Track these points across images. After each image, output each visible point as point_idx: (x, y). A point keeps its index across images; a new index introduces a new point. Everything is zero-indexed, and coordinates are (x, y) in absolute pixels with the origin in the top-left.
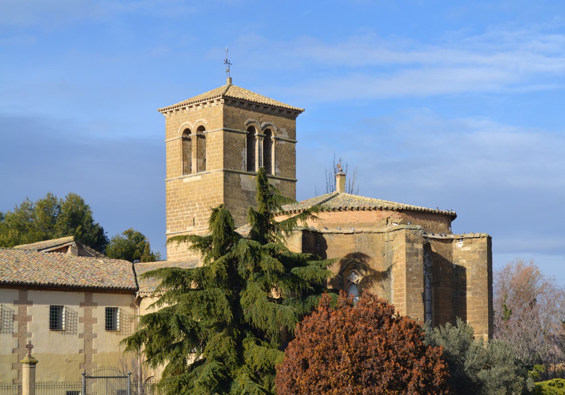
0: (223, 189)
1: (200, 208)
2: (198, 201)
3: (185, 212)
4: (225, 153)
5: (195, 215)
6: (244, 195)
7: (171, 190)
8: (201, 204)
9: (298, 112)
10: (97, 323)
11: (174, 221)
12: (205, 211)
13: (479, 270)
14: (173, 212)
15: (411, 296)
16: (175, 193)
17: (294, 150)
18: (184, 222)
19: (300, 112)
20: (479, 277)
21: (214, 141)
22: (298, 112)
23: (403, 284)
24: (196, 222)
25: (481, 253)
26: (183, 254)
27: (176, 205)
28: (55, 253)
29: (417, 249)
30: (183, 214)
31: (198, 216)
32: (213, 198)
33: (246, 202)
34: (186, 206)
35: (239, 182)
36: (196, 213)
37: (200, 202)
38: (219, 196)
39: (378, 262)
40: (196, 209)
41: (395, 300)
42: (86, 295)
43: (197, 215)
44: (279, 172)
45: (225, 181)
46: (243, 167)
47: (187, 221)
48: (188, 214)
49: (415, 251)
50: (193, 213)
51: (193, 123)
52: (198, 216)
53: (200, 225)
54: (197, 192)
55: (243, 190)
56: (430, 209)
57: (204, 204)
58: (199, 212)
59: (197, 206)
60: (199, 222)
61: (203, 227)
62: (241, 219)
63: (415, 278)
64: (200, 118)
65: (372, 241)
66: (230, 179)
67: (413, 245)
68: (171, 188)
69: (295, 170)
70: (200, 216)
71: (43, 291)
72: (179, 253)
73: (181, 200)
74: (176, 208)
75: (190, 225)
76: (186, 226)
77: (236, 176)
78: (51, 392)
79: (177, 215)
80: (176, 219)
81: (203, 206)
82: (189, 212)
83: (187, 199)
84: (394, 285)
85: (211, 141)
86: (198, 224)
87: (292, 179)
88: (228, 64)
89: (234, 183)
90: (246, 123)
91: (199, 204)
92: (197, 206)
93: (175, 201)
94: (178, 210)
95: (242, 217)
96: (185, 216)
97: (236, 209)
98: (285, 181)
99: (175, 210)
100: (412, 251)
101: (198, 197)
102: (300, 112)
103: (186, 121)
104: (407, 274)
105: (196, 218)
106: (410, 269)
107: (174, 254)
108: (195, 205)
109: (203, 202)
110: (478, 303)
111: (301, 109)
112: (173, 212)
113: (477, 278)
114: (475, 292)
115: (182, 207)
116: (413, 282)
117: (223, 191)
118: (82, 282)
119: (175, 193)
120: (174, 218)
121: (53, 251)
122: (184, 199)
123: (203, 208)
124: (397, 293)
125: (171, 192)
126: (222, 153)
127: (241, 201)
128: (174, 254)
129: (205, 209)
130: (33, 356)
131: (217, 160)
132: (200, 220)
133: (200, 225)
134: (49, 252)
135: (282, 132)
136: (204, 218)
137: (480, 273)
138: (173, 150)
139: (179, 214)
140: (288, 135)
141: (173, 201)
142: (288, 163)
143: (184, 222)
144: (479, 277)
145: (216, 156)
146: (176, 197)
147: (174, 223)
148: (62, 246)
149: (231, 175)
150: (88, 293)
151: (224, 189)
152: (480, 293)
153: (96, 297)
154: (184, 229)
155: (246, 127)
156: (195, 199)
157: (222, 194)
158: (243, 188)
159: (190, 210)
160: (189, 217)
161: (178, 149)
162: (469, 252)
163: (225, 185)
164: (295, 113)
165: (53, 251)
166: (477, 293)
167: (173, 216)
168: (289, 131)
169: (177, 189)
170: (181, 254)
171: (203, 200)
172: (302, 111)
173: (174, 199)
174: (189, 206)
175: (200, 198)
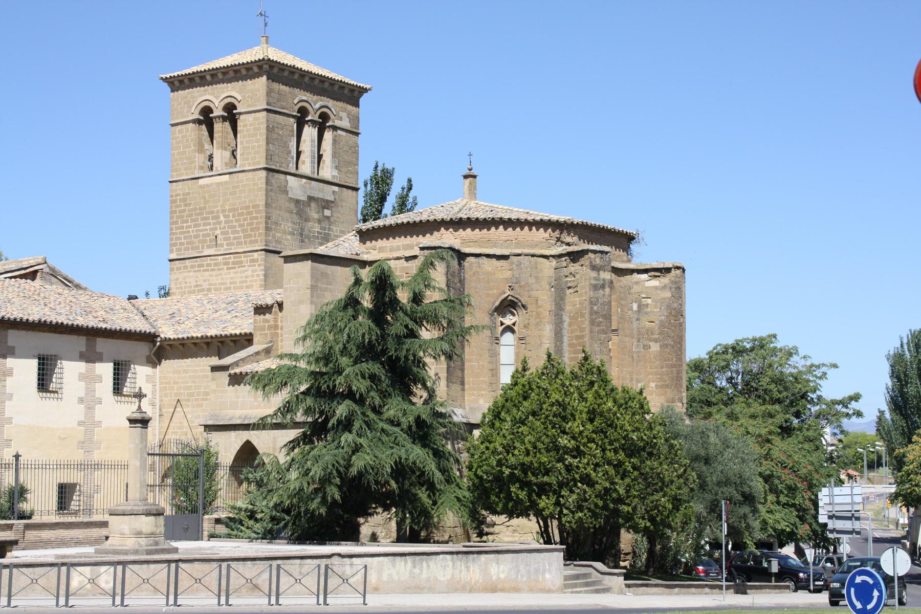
0: (264, 195)
1: (226, 222)
2: (223, 211)
3: (201, 228)
4: (268, 143)
5: (218, 232)
6: (292, 206)
7: (179, 195)
8: (228, 216)
9: (363, 91)
10: (101, 382)
11: (183, 241)
12: (235, 227)
13: (670, 313)
14: (182, 227)
15: (596, 345)
16: (184, 200)
17: (357, 145)
18: (199, 242)
19: (366, 90)
20: (670, 323)
21: (251, 125)
22: (363, 91)
23: (584, 328)
24: (219, 242)
25: (673, 289)
26: (197, 289)
27: (187, 217)
28: (18, 279)
29: (604, 280)
30: (197, 231)
31: (222, 233)
32: (248, 207)
33: (294, 216)
34: (193, 221)
35: (286, 186)
36: (220, 228)
37: (227, 213)
38: (258, 206)
39: (543, 297)
40: (220, 223)
41: (570, 351)
42: (87, 340)
43: (221, 232)
44: (337, 174)
45: (267, 183)
46: (291, 165)
47: (205, 241)
48: (206, 230)
49: (601, 282)
50: (216, 228)
51: (217, 98)
52: (222, 233)
53: (225, 247)
54: (221, 199)
55: (291, 198)
56: (609, 227)
57: (234, 216)
58: (224, 228)
59: (222, 218)
60: (225, 243)
61: (231, 249)
62: (287, 239)
63: (601, 320)
64: (228, 91)
65: (536, 268)
66: (273, 181)
67: (599, 274)
68: (178, 192)
69: (357, 173)
70: (226, 234)
71: (29, 332)
72: (191, 287)
73: (195, 209)
74: (187, 222)
75: (209, 247)
76: (203, 248)
77: (282, 176)
78: (65, 479)
79: (197, 231)
80: (185, 238)
81: (231, 218)
82: (208, 227)
83: (205, 208)
84: (568, 330)
85: (245, 126)
86: (222, 245)
87: (353, 186)
88: (263, 17)
89: (279, 187)
90: (296, 101)
91: (225, 216)
92: (222, 218)
93: (184, 211)
94: (189, 224)
95: (289, 237)
96: (201, 233)
97: (281, 224)
98: (345, 189)
99: (185, 225)
100: (597, 282)
101: (222, 206)
102: (366, 90)
103: (205, 95)
104: (591, 314)
105: (219, 237)
106: (595, 308)
107: (181, 288)
108: (218, 217)
109: (231, 214)
110: (669, 360)
111: (368, 87)
112: (182, 227)
113: (667, 325)
114: (664, 344)
115: (196, 220)
116: (599, 326)
117: (264, 198)
118: (80, 321)
119: (184, 200)
120: (182, 236)
121: (15, 277)
122: (200, 209)
123: (232, 221)
124: (574, 341)
125: (179, 197)
126: (263, 143)
127: (288, 214)
128: (181, 288)
129: (234, 224)
130: (144, 410)
131: (255, 153)
132: (225, 239)
133: (225, 247)
134: (11, 278)
135: (341, 117)
136: (232, 236)
137: (672, 318)
138: (183, 137)
139: (191, 230)
140: (350, 122)
141: (180, 212)
142: (350, 163)
143: (199, 242)
144: (670, 323)
145: (253, 147)
146: (186, 205)
147: (182, 244)
148: (28, 271)
149: (277, 175)
150: (90, 337)
151: (266, 195)
152: (671, 345)
153: (101, 344)
154: (198, 252)
155: (297, 108)
156: (219, 208)
157: (262, 203)
158: (290, 195)
159: (209, 224)
160: (208, 235)
161: (190, 135)
162: (656, 288)
163: (267, 191)
164: (360, 92)
165: (15, 277)
166: (667, 345)
167: (180, 233)
168: (351, 117)
169: (188, 194)
170: (193, 288)
171: (230, 211)
172: (369, 89)
173: (183, 208)
174: (207, 218)
175: (227, 207)
